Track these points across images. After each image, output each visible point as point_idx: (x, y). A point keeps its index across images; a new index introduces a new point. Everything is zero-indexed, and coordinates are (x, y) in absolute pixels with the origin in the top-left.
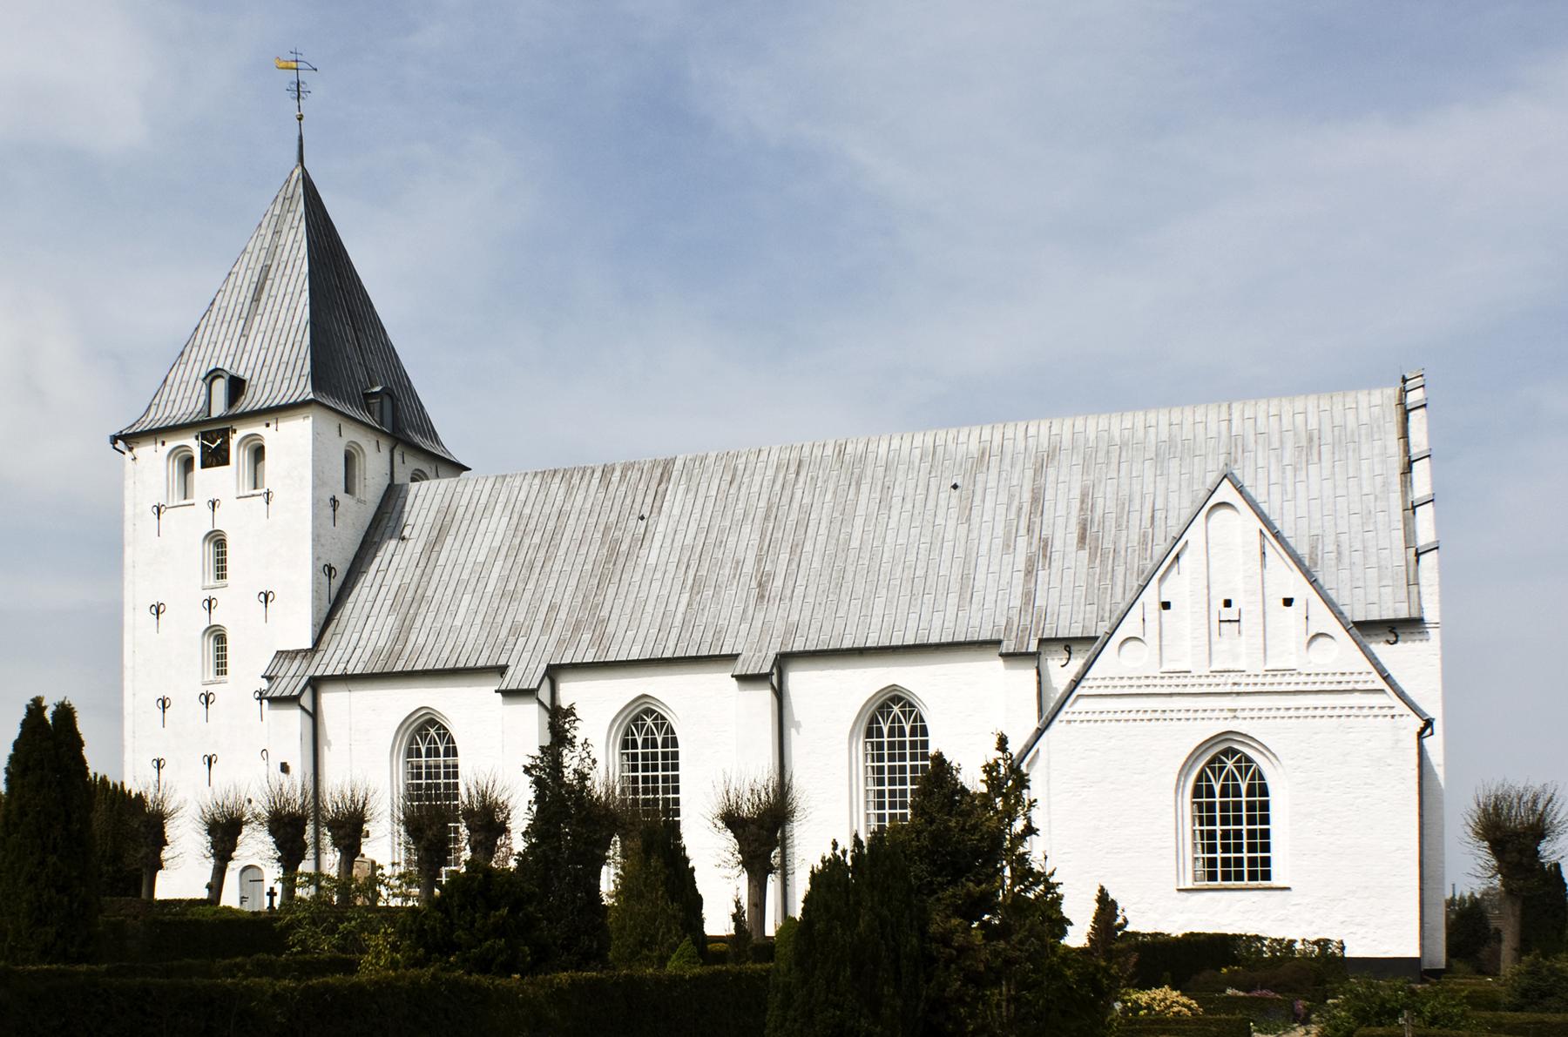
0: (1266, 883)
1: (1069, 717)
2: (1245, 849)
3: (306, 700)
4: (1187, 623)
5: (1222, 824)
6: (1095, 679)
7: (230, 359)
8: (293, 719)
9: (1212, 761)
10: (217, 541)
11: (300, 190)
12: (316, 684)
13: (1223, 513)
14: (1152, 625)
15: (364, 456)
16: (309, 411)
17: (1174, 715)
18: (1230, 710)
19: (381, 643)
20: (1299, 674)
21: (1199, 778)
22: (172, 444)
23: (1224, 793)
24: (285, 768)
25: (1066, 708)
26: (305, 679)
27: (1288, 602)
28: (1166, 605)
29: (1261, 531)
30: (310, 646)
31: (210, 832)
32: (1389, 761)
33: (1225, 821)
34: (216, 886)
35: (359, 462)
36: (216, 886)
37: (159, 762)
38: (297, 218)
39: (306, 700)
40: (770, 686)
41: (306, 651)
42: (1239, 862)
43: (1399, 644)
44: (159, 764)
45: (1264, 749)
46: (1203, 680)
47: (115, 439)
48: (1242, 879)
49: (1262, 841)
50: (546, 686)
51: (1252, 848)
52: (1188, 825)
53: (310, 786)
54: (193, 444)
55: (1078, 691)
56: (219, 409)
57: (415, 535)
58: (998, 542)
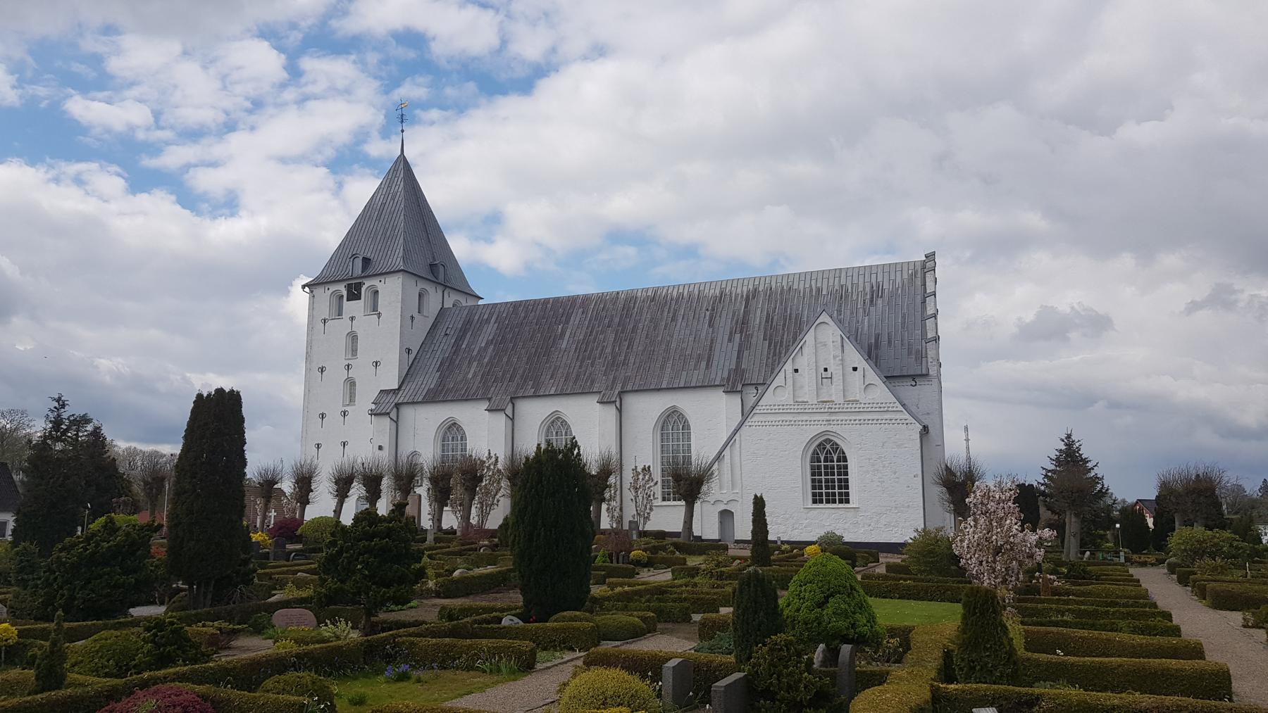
0: (847, 506)
1: (750, 424)
2: (836, 488)
3: (393, 415)
4: (807, 378)
5: (825, 476)
6: (762, 406)
7: (373, 254)
8: (386, 422)
9: (819, 445)
10: (353, 337)
11: (402, 166)
12: (398, 406)
13: (823, 326)
15: (429, 294)
16: (402, 273)
18: (827, 421)
19: (432, 386)
20: (861, 403)
21: (813, 454)
22: (333, 288)
24: (380, 448)
25: (748, 419)
26: (394, 404)
27: (855, 369)
28: (796, 371)
29: (841, 335)
30: (397, 387)
31: (336, 483)
33: (826, 474)
34: (338, 511)
36: (338, 511)
37: (318, 445)
38: (399, 180)
39: (393, 415)
40: (615, 407)
42: (834, 494)
43: (918, 387)
44: (318, 446)
49: (845, 484)
51: (840, 488)
53: (510, 453)
54: (342, 288)
57: (452, 333)
58: (726, 338)
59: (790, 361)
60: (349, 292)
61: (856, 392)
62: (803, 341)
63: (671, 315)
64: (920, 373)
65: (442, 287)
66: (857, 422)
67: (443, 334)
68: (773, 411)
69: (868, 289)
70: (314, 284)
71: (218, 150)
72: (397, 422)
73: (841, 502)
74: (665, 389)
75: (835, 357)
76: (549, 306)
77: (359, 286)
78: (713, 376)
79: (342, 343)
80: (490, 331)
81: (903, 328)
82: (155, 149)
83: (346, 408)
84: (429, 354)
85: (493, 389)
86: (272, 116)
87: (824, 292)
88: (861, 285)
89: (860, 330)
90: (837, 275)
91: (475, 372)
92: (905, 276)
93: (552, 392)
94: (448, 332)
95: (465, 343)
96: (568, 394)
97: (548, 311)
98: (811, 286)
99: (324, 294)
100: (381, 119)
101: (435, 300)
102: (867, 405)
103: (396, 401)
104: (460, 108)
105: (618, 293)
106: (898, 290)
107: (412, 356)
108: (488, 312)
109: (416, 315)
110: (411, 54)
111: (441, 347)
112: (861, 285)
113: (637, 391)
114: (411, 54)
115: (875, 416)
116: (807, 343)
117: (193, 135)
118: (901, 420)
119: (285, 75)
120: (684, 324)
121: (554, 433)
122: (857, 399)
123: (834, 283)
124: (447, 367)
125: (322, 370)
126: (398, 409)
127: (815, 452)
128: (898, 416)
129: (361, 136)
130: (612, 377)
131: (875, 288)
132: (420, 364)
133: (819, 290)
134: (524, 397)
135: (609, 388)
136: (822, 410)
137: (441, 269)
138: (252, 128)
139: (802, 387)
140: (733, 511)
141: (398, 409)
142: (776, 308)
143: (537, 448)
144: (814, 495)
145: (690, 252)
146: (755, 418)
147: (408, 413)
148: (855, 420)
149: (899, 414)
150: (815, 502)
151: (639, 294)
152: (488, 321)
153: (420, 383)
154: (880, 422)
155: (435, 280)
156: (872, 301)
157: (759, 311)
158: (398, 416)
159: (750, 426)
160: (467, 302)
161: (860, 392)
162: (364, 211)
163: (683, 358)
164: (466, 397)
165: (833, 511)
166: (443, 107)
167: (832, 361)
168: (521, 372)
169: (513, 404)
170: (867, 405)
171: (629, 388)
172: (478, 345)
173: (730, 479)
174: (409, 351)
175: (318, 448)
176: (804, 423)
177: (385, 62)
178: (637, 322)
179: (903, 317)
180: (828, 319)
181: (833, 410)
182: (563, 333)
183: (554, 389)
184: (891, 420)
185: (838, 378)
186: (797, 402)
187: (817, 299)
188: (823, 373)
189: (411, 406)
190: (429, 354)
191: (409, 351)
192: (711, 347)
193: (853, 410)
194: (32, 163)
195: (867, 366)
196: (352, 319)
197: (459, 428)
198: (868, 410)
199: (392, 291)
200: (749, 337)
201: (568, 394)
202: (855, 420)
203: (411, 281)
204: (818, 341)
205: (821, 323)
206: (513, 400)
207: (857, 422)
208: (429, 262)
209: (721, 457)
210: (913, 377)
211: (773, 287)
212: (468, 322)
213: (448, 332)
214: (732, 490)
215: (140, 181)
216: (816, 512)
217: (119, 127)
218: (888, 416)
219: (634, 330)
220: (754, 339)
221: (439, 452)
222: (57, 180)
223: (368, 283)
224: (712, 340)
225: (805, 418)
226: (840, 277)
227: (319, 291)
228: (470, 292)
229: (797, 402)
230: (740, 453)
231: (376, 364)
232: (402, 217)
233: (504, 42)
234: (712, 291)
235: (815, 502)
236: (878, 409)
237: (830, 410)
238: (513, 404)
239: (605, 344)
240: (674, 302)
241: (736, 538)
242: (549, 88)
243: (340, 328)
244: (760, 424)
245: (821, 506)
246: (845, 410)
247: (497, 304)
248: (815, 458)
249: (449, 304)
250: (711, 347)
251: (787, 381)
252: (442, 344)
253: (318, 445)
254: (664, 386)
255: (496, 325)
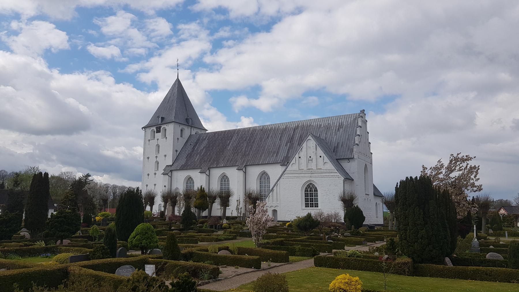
0: (317, 208)
1: (283, 177)
3: (170, 174)
4: (303, 160)
8: (167, 177)
10: (158, 146)
12: (171, 171)
13: (310, 140)
14: (297, 161)
16: (173, 123)
17: (301, 177)
18: (310, 176)
20: (322, 170)
22: (152, 128)
23: (310, 191)
24: (165, 186)
25: (283, 176)
27: (320, 157)
30: (172, 164)
32: (338, 185)
35: (184, 131)
39: (244, 170)
41: (171, 165)
43: (350, 163)
44: (155, 185)
45: (316, 183)
46: (306, 171)
47: (142, 128)
48: (309, 207)
49: (317, 200)
50: (244, 168)
52: (304, 197)
53: (170, 189)
55: (285, 173)
56: (160, 122)
58: (285, 144)
59: (297, 154)
60: (157, 130)
61: (321, 165)
62: (302, 146)
63: (267, 136)
64: (351, 157)
65: (190, 127)
66: (321, 177)
67: (189, 144)
68: (291, 173)
69: (338, 125)
70: (146, 127)
71: (147, 65)
72: (171, 177)
73: (315, 207)
74: (260, 164)
75: (313, 152)
76: (226, 133)
77: (160, 127)
78: (278, 159)
79: (154, 148)
80: (205, 142)
81: (348, 140)
82: (123, 65)
83: (156, 172)
84: (184, 152)
85: (203, 165)
86: (167, 49)
87: (322, 126)
88: (336, 123)
89: (332, 141)
90: (328, 120)
91: (198, 158)
92: (352, 119)
93: (222, 166)
94: (191, 144)
95: (196, 148)
96: (228, 166)
97: (226, 135)
98: (318, 124)
99: (149, 131)
100: (211, 47)
101: (187, 132)
102: (324, 170)
103: (171, 169)
104: (239, 40)
105: (250, 128)
106: (348, 125)
107: (178, 153)
108: (206, 136)
109: (179, 137)
110: (222, 17)
111: (188, 149)
112: (336, 123)
113: (251, 165)
114: (222, 17)
115: (327, 174)
116: (303, 147)
117: (137, 59)
118: (336, 176)
119: (171, 33)
120: (271, 140)
121: (267, 178)
122: (321, 168)
123: (326, 123)
124: (190, 156)
125: (148, 158)
126: (171, 172)
127: (306, 188)
128: (336, 174)
129: (203, 54)
130: (243, 160)
131: (340, 124)
132: (180, 156)
133: (320, 125)
134: (213, 168)
135: (242, 164)
136: (308, 172)
137: (190, 120)
138: (160, 55)
139: (302, 164)
140: (277, 210)
141: (171, 172)
142: (304, 133)
143: (201, 187)
144: (306, 204)
145: (343, 98)
146: (285, 175)
147: (175, 174)
148: (320, 176)
149: (336, 173)
150: (306, 207)
151: (257, 128)
152: (205, 139)
153: (179, 163)
154: (329, 176)
155: (188, 125)
156: (338, 130)
157: (298, 134)
158: (171, 175)
159: (283, 178)
160: (200, 132)
161: (322, 165)
162: (164, 100)
163: (268, 152)
164: (194, 168)
165: (312, 210)
166: (234, 39)
167: (312, 154)
168: (213, 158)
169: (209, 170)
170: (324, 170)
171: (248, 164)
172: (200, 149)
173: (276, 198)
174: (177, 151)
175: (147, 186)
176: (302, 177)
177: (212, 21)
178: (255, 139)
179: (349, 136)
180: (311, 138)
181: (312, 172)
182: (229, 143)
183: (223, 164)
184: (333, 176)
185: (314, 160)
186: (300, 169)
187: (319, 128)
188: (309, 158)
189: (176, 171)
190: (184, 152)
191: (177, 151)
192: (279, 148)
193: (319, 172)
194: (82, 72)
195: (325, 156)
196: (158, 139)
197: (192, 179)
198: (325, 172)
199: (170, 128)
200: (293, 144)
201: (228, 166)
202: (320, 176)
203: (177, 126)
204: (308, 146)
205: (309, 139)
206: (209, 169)
207: (321, 177)
208: (186, 118)
209: (273, 190)
210: (348, 159)
211: (304, 125)
212: (198, 140)
213: (191, 144)
214: (277, 202)
215: (120, 79)
216: (306, 210)
217: (109, 56)
218: (332, 174)
219: (253, 142)
220: (295, 145)
221: (185, 186)
222: (91, 78)
223: (163, 126)
224: (280, 145)
225: (302, 175)
226: (329, 120)
227: (147, 130)
228: (203, 129)
229: (300, 169)
230: (280, 188)
231: (165, 156)
232: (176, 102)
233: (259, 9)
234: (283, 127)
235: (306, 207)
236: (328, 172)
237: (311, 172)
238: (209, 170)
239: (243, 147)
240: (269, 131)
241: (278, 220)
242: (278, 28)
243: (154, 142)
244: (286, 177)
245: (308, 208)
246: (316, 172)
247: (209, 133)
248: (306, 190)
249: (193, 133)
250: (279, 148)
251: (296, 161)
252: (189, 148)
253: (147, 185)
254: (260, 163)
255: (207, 141)
